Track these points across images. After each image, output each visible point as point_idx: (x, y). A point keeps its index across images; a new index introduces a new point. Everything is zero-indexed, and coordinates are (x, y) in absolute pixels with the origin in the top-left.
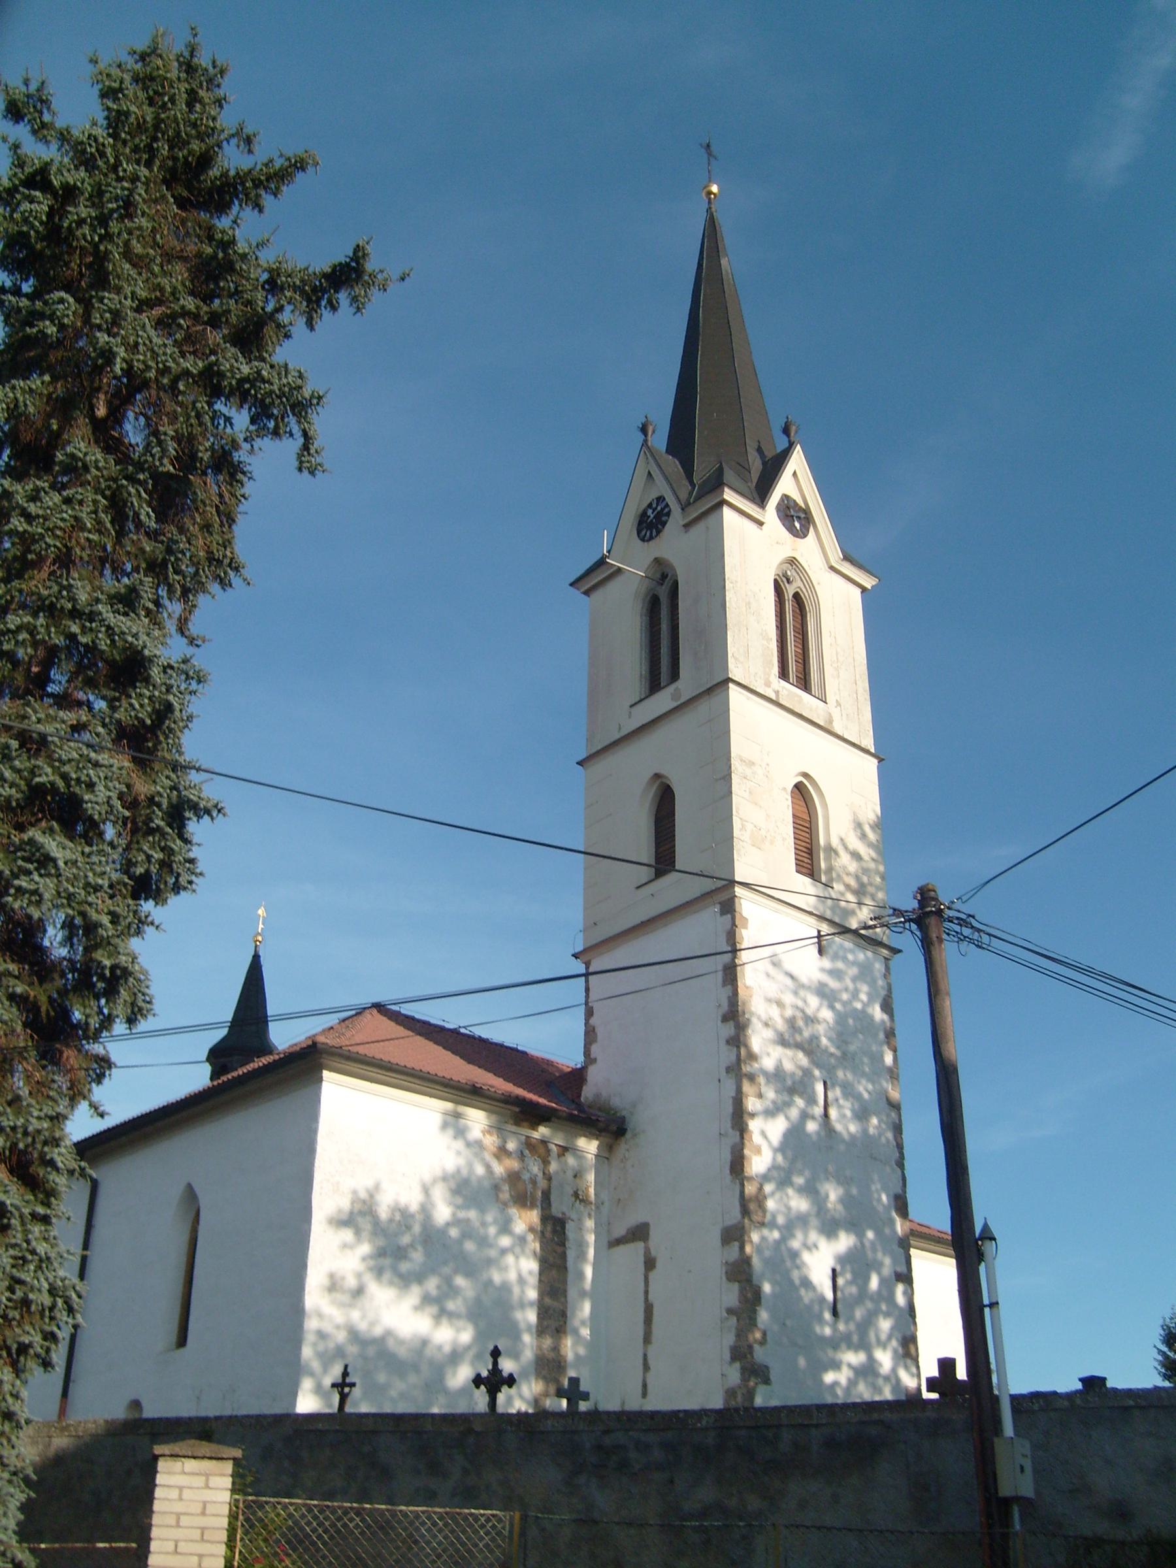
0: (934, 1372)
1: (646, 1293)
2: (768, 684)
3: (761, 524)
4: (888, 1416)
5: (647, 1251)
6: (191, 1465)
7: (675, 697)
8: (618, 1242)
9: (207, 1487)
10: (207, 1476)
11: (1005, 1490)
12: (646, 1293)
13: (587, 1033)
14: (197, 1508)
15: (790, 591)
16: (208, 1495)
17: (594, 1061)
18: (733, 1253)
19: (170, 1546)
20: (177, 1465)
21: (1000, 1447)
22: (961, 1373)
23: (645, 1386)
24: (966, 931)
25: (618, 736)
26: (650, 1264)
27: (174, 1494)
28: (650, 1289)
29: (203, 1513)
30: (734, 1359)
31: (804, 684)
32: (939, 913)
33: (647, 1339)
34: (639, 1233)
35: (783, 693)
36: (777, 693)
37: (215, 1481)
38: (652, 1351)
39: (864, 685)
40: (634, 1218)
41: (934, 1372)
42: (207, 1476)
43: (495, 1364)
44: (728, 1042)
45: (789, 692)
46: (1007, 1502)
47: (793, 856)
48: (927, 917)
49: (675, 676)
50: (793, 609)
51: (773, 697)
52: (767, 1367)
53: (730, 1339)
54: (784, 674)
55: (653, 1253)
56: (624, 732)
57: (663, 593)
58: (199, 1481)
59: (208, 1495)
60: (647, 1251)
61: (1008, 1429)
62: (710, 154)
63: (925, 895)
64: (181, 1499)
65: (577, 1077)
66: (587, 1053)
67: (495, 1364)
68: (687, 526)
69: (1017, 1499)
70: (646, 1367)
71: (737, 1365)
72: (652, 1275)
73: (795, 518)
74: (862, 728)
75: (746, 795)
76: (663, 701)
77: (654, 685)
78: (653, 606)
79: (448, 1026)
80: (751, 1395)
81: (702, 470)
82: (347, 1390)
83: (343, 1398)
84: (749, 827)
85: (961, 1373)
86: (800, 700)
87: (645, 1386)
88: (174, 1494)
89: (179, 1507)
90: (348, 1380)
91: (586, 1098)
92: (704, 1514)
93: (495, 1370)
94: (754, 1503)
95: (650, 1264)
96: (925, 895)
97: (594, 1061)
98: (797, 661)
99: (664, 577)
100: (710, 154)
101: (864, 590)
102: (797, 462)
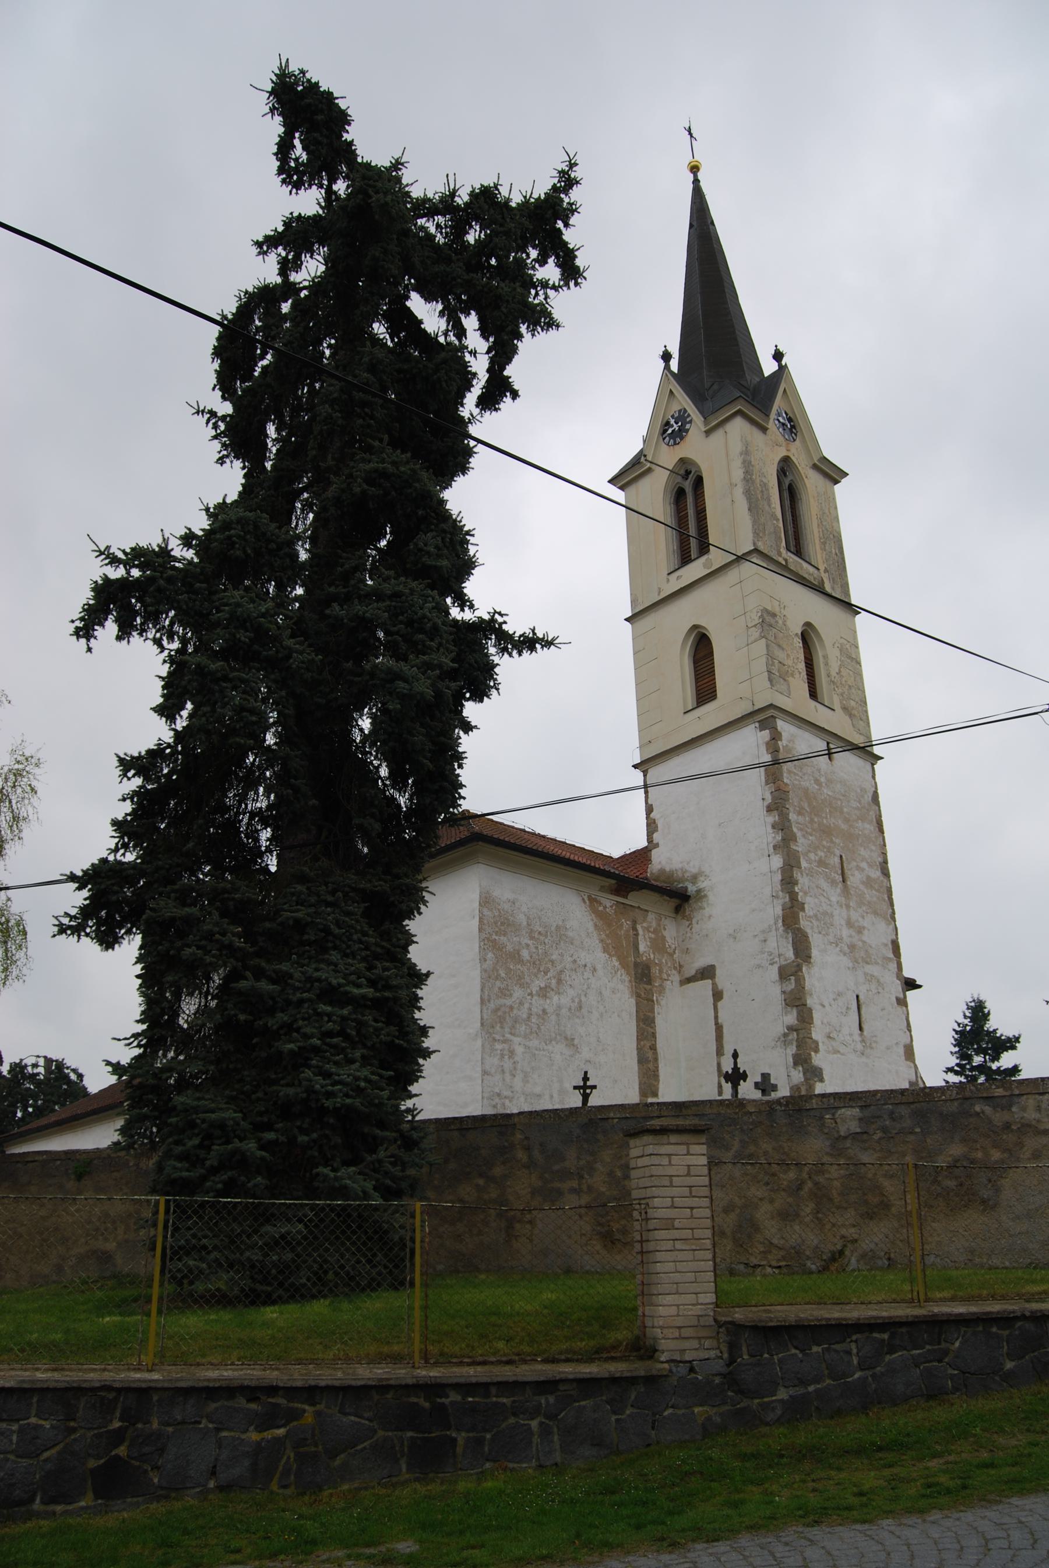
0: (759, 1079)
1: (716, 1018)
2: (780, 554)
5: (714, 985)
8: (689, 980)
9: (688, 1154)
12: (716, 1018)
13: (648, 825)
14: (683, 1171)
17: (657, 845)
18: (791, 985)
26: (718, 995)
28: (719, 1014)
29: (688, 1174)
36: (786, 560)
40: (701, 962)
41: (759, 1079)
43: (735, 1063)
44: (773, 827)
45: (792, 558)
52: (821, 1069)
53: (792, 1050)
56: (663, 595)
57: (688, 486)
58: (682, 1149)
60: (714, 985)
62: (690, 134)
64: (670, 1164)
65: (641, 857)
66: (650, 839)
67: (735, 1063)
68: (708, 433)
72: (720, 1004)
76: (696, 570)
77: (685, 559)
78: (679, 495)
79: (516, 826)
80: (811, 1087)
82: (588, 1091)
83: (586, 1097)
86: (802, 568)
89: (671, 1171)
90: (588, 1083)
91: (652, 873)
94: (996, 1155)
95: (718, 995)
97: (657, 845)
99: (688, 473)
100: (690, 134)
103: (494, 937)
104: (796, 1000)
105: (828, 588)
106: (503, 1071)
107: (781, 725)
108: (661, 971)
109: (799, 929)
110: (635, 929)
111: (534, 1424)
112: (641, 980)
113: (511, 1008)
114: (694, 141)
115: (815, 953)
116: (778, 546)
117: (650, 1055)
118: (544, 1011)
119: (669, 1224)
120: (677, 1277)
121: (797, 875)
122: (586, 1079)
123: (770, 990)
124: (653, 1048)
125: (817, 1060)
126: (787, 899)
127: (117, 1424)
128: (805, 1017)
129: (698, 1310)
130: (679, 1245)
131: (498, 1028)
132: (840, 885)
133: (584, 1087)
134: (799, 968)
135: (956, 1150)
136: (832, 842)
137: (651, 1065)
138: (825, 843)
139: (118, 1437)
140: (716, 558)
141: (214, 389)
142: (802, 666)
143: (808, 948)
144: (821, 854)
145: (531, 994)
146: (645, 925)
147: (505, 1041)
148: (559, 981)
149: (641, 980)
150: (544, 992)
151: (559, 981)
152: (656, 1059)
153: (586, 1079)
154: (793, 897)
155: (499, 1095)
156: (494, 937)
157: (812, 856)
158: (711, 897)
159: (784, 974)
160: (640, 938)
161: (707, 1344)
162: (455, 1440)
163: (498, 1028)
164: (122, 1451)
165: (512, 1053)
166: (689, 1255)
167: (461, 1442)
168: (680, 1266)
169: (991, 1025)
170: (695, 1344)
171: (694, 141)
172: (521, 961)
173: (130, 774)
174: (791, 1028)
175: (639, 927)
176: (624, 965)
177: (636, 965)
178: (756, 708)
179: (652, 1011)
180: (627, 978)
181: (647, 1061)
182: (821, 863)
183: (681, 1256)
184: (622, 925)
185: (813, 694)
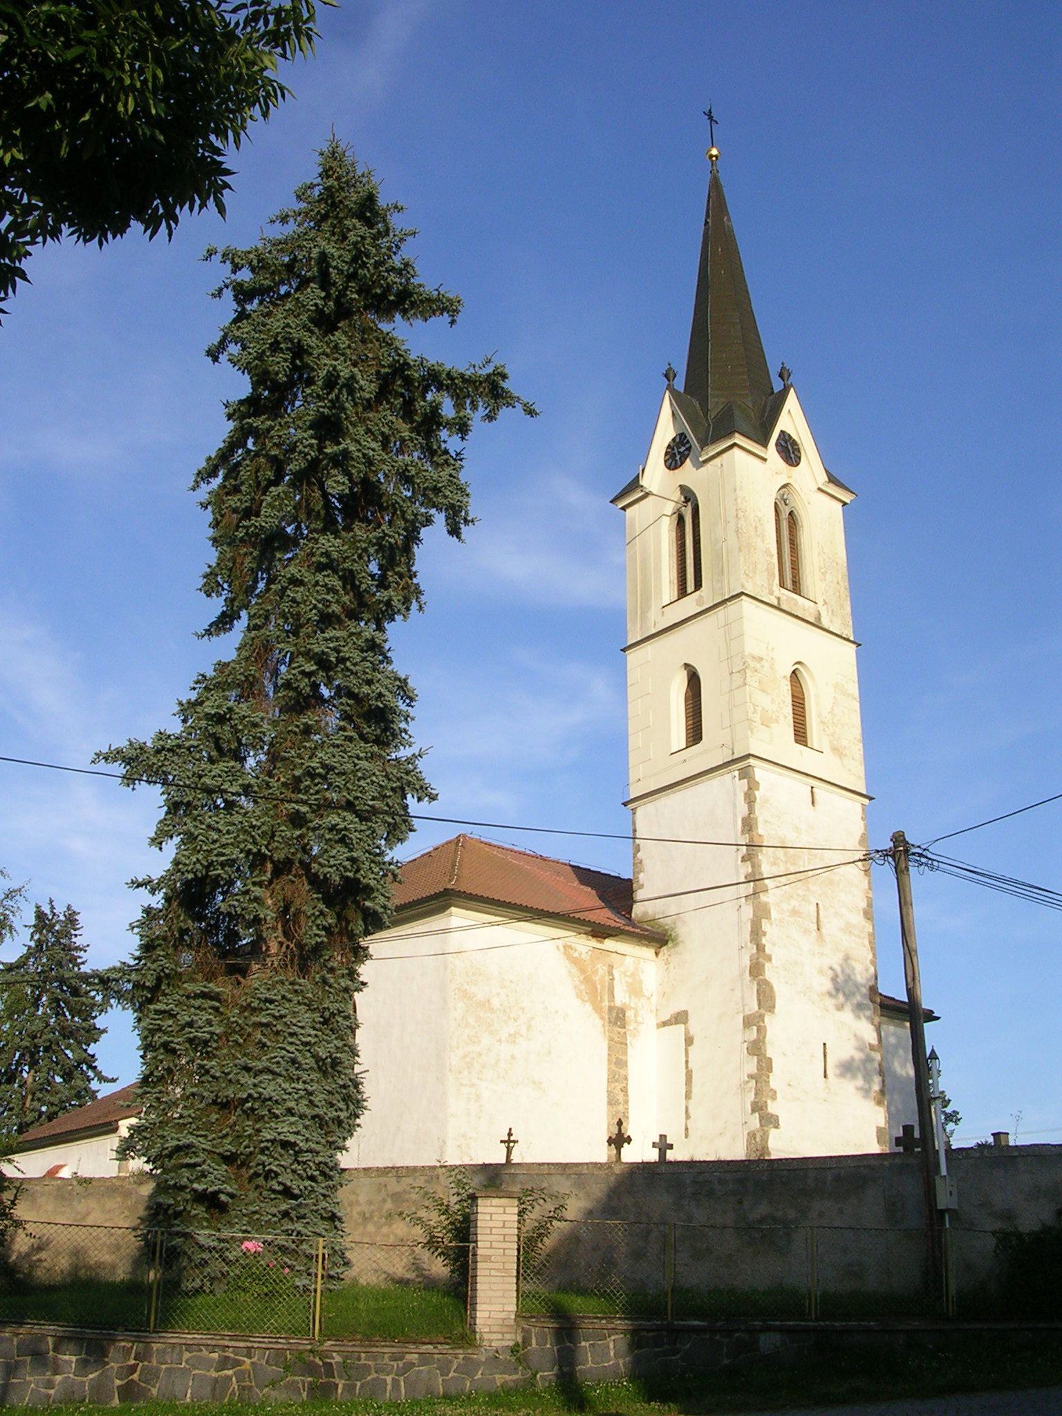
1: (687, 1062)
2: (771, 593)
3: (765, 460)
4: (872, 1162)
6: (496, 1201)
7: (699, 602)
10: (504, 1207)
11: (941, 1206)
12: (687, 1062)
15: (785, 515)
16: (505, 1217)
18: (753, 1034)
19: (488, 1245)
20: (488, 1201)
21: (938, 1181)
22: (917, 1134)
23: (687, 1129)
24: (923, 860)
25: (654, 631)
27: (488, 1217)
30: (753, 1111)
31: (796, 588)
32: (906, 851)
33: (688, 1096)
34: (680, 1018)
35: (783, 598)
37: (508, 1210)
38: (692, 1103)
39: (845, 584)
42: (504, 1207)
43: (620, 1130)
46: (942, 1212)
47: (792, 729)
48: (900, 854)
49: (698, 585)
50: (789, 524)
51: (775, 603)
53: (751, 1097)
54: (782, 585)
55: (692, 1033)
59: (505, 1217)
60: (687, 1032)
61: (944, 1172)
62: (711, 118)
63: (899, 838)
67: (620, 1130)
69: (948, 1210)
70: (688, 1116)
71: (757, 1115)
73: (790, 451)
74: (841, 621)
75: (756, 685)
76: (690, 605)
77: (683, 592)
81: (716, 403)
83: (509, 1150)
84: (759, 709)
85: (917, 1134)
86: (796, 603)
87: (687, 1129)
88: (488, 1217)
89: (491, 1224)
92: (761, 1221)
93: (620, 1134)
94: (792, 1214)
95: (689, 1041)
96: (899, 838)
98: (792, 575)
100: (711, 118)
101: (845, 504)
102: (792, 402)
103: (465, 986)
104: (756, 1048)
105: (825, 622)
106: (469, 1114)
107: (761, 772)
108: (636, 1015)
109: (767, 983)
110: (611, 973)
111: (389, 1379)
112: (616, 1023)
113: (480, 1054)
114: (714, 125)
115: (779, 1003)
116: (771, 585)
117: (621, 1097)
118: (513, 1057)
119: (488, 1258)
120: (491, 1293)
121: (765, 925)
122: (510, 1134)
123: (739, 1038)
124: (625, 1090)
125: (772, 1108)
126: (755, 951)
127: (132, 1362)
128: (765, 1066)
129: (503, 1315)
130: (493, 1272)
131: (466, 1072)
132: (814, 933)
133: (509, 1141)
134: (761, 1017)
135: (763, 1209)
136: (808, 889)
137: (621, 1108)
138: (799, 891)
139: (133, 1369)
140: (706, 596)
141: (219, 293)
142: (788, 710)
143: (772, 997)
144: (794, 903)
145: (500, 1041)
146: (622, 969)
147: (473, 1085)
148: (529, 1027)
149: (616, 1023)
150: (513, 1038)
151: (529, 1027)
152: (627, 1102)
153: (510, 1134)
154: (760, 948)
155: (463, 1136)
156: (465, 986)
157: (785, 906)
158: (680, 948)
159: (748, 1022)
160: (616, 982)
161: (508, 1336)
162: (337, 1385)
163: (466, 1072)
164: (135, 1376)
165: (478, 1097)
166: (501, 1280)
167: (340, 1386)
168: (494, 1287)
169: (625, 1145)
170: (500, 1336)
171: (714, 125)
172: (492, 1010)
173: (136, 930)
174: (751, 1077)
175: (615, 972)
176: (597, 1009)
177: (611, 1009)
178: (736, 756)
179: (625, 1053)
180: (599, 1023)
181: (617, 1103)
182: (795, 912)
183: (494, 1280)
184: (597, 971)
185: (801, 736)
